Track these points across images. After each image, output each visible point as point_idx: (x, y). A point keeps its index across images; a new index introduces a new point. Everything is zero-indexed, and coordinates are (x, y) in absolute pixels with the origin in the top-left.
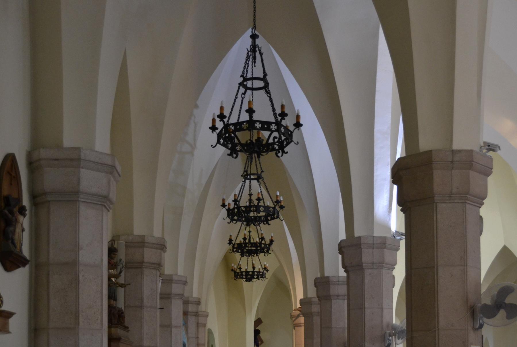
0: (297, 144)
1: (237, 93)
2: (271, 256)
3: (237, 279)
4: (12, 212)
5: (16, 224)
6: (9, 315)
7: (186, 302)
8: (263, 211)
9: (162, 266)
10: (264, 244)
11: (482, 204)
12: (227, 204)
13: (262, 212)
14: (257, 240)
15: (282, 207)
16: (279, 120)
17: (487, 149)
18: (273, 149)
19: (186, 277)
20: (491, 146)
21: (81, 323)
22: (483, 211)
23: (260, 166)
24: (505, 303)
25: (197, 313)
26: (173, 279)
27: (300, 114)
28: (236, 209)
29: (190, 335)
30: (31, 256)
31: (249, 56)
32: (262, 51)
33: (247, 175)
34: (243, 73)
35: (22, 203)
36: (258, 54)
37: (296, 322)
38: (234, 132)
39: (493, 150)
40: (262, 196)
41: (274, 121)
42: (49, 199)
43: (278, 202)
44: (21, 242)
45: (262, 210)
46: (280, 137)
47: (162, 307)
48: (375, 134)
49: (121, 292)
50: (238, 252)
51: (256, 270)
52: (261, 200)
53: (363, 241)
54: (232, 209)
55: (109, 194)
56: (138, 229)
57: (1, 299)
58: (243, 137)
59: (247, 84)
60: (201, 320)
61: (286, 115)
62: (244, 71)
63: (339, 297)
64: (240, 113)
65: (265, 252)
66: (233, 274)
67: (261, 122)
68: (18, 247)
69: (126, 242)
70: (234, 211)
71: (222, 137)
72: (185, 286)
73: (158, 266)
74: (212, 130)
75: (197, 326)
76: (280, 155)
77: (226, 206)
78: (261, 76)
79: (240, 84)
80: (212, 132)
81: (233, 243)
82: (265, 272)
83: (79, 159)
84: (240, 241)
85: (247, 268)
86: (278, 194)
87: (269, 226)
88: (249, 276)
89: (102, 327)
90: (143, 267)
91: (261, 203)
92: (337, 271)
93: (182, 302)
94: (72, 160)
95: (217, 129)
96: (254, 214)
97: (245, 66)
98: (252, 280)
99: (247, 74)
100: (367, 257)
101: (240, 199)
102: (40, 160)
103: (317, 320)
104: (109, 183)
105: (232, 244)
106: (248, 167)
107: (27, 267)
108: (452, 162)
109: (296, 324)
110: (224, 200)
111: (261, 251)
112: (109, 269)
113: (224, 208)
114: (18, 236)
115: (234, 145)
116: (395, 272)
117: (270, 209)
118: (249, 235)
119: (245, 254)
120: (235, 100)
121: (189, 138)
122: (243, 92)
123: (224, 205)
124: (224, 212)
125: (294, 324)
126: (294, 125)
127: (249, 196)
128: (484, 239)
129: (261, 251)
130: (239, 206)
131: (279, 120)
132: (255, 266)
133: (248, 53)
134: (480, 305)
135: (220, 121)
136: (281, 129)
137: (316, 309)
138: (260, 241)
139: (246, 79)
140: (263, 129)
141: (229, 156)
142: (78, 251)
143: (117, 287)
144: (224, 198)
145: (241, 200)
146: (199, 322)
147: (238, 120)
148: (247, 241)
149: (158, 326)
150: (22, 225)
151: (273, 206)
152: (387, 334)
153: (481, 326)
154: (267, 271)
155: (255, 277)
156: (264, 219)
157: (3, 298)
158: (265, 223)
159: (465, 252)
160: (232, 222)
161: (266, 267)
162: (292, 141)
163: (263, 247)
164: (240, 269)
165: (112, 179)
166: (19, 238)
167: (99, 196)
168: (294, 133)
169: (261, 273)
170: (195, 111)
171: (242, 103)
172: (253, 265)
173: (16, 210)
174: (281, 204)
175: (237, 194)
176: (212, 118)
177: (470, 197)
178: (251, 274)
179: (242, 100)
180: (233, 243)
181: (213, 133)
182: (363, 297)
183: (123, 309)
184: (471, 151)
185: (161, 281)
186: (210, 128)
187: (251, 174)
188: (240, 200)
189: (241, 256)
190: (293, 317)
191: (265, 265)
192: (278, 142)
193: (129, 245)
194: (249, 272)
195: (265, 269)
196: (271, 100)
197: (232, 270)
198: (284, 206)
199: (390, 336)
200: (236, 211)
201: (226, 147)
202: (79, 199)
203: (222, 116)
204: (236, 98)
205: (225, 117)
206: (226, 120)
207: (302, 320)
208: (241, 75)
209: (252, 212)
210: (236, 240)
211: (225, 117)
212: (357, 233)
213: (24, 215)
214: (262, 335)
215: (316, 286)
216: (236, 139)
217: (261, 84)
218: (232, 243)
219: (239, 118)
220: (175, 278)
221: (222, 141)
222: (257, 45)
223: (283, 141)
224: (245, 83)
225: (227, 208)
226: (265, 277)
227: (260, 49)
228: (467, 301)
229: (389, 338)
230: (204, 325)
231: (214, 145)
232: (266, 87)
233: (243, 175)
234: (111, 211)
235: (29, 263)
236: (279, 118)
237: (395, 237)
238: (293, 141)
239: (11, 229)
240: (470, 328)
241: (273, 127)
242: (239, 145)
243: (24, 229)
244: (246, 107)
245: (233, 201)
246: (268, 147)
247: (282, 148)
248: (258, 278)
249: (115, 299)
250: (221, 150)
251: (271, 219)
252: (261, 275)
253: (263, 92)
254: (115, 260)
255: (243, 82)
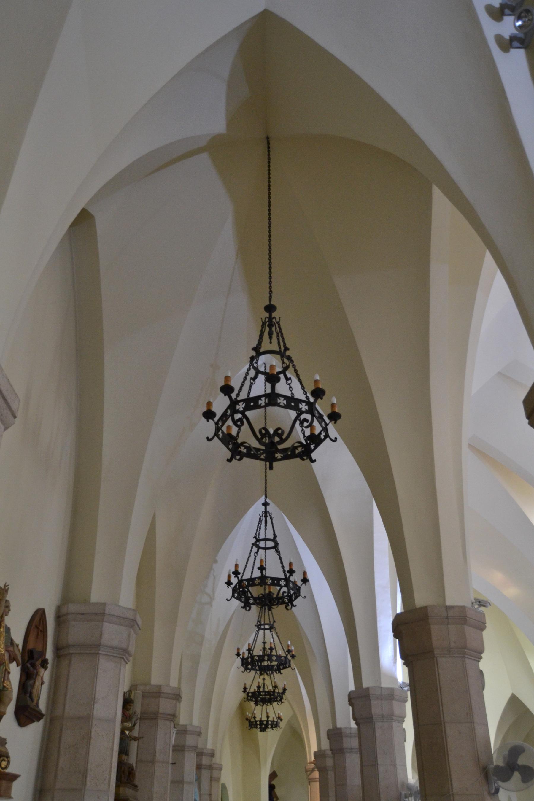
0: (305, 597)
1: (251, 552)
2: (285, 704)
3: (251, 729)
4: (33, 665)
5: (36, 677)
6: (14, 777)
7: (200, 754)
8: (276, 661)
9: (176, 717)
10: (277, 693)
11: (481, 658)
12: (241, 653)
13: (274, 661)
14: (271, 688)
15: (293, 656)
16: (288, 576)
17: (478, 605)
18: (283, 603)
19: (200, 728)
20: (482, 602)
21: (88, 783)
22: (483, 665)
23: (273, 616)
24: (518, 765)
25: (210, 766)
26: (188, 730)
27: (307, 571)
28: (249, 658)
29: (202, 792)
30: (47, 711)
31: (261, 520)
32: (272, 516)
33: (261, 625)
34: (256, 535)
35: (45, 656)
36: (268, 519)
37: (311, 777)
38: (247, 587)
39: (484, 606)
40: (274, 645)
41: (284, 577)
42: (71, 652)
43: (289, 651)
44: (39, 696)
45: (274, 660)
46: (289, 592)
47: (174, 763)
48: (376, 587)
49: (134, 746)
50: (252, 700)
51: (271, 719)
52: (273, 649)
53: (371, 692)
54: (246, 658)
55: (128, 647)
56: (156, 680)
57: (9, 759)
58: (256, 591)
59: (259, 544)
60: (215, 774)
61: (294, 572)
62: (256, 533)
63: (352, 751)
64: (253, 569)
65: (279, 701)
66: (247, 723)
67: (272, 578)
68: (35, 701)
69: (143, 692)
70: (248, 660)
71: (237, 591)
72: (199, 737)
73: (173, 717)
74: (227, 584)
75: (211, 781)
76: (289, 608)
77: (241, 655)
78: (272, 537)
79: (253, 544)
80: (228, 586)
81: (248, 692)
82: (279, 721)
83: (103, 614)
84: (255, 689)
85: (262, 717)
86: (289, 644)
87: (282, 675)
88: (263, 726)
89: (109, 788)
90: (158, 719)
91: (274, 653)
92: (349, 722)
93: (195, 755)
94: (96, 614)
95: (232, 584)
96: (268, 663)
97: (257, 529)
98: (267, 730)
99: (259, 535)
100: (377, 708)
101: (254, 648)
102: (67, 614)
103: (331, 774)
104: (129, 636)
105: (246, 692)
106: (261, 618)
107: (42, 721)
108: (447, 617)
109: (311, 779)
110: (238, 649)
111: (274, 699)
112: (122, 722)
113: (238, 657)
114: (37, 690)
115: (247, 599)
116: (404, 725)
117: (282, 659)
118: (263, 682)
119: (259, 703)
120: (249, 558)
121: (209, 590)
122: (256, 551)
123: (238, 654)
124: (239, 661)
125: (309, 779)
126: (302, 581)
127: (263, 644)
128: (487, 694)
129: (274, 699)
130: (252, 655)
131: (288, 576)
132: (270, 715)
133: (260, 518)
134: (493, 766)
135: (235, 577)
136: (289, 584)
137: (329, 762)
138: (273, 690)
139: (258, 540)
140: (273, 584)
141: (243, 609)
142: (94, 705)
143: (130, 740)
144: (239, 647)
145: (255, 649)
146: (213, 777)
147: (251, 576)
148: (261, 689)
149: (169, 783)
150: (42, 678)
151: (285, 655)
152: (403, 795)
153: (497, 791)
154: (281, 720)
155: (270, 726)
156: (277, 668)
157: (10, 759)
158: (277, 672)
159: (470, 707)
160: (246, 671)
161: (280, 716)
162: (300, 595)
163: (276, 695)
164: (255, 718)
165: (132, 632)
166: (37, 692)
167: (119, 649)
168: (301, 588)
169: (275, 723)
170: (215, 566)
171: (255, 561)
172: (267, 713)
173: (38, 663)
174: (292, 653)
175: (250, 644)
176: (228, 574)
177: (468, 651)
178: (266, 722)
179: (255, 558)
180: (248, 692)
181: (228, 587)
182: (375, 752)
183: (134, 765)
184: (463, 607)
185: (175, 732)
186: (226, 583)
187: (264, 624)
188: (254, 649)
189: (255, 705)
190: (307, 771)
191: (279, 714)
192: (287, 596)
193: (146, 695)
194: (264, 721)
195: (279, 718)
196: (280, 558)
197: (247, 719)
198: (295, 655)
199: (406, 797)
200: (249, 660)
201: (241, 601)
202: (100, 652)
203: (236, 573)
204: (249, 556)
205: (239, 573)
206: (240, 576)
207: (316, 774)
208: (254, 536)
209: (266, 661)
210: (250, 688)
211: (239, 573)
212: (366, 684)
213: (46, 668)
214: (277, 791)
215: (328, 738)
216: (249, 593)
217: (271, 544)
218: (246, 691)
219: (252, 574)
220: (189, 728)
221: (236, 595)
222: (268, 511)
223: (291, 596)
224: (258, 543)
225: (241, 657)
226: (279, 727)
227: (271, 514)
228: (479, 761)
229: (405, 800)
230: (218, 779)
231: (229, 599)
232: (276, 547)
233: (257, 625)
234: (129, 663)
235: (44, 717)
236: (288, 575)
237: (402, 688)
238: (301, 595)
239: (31, 682)
240: (486, 793)
241: (283, 583)
242: (252, 599)
243: (43, 681)
244: (258, 565)
245: (247, 650)
246: (279, 600)
247: (291, 601)
248: (272, 727)
249: (127, 754)
250: (236, 603)
251: (284, 668)
252: (275, 725)
253: (273, 551)
254: (131, 712)
255: (256, 542)
